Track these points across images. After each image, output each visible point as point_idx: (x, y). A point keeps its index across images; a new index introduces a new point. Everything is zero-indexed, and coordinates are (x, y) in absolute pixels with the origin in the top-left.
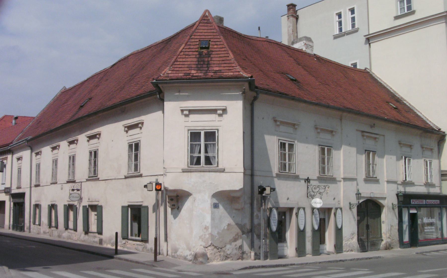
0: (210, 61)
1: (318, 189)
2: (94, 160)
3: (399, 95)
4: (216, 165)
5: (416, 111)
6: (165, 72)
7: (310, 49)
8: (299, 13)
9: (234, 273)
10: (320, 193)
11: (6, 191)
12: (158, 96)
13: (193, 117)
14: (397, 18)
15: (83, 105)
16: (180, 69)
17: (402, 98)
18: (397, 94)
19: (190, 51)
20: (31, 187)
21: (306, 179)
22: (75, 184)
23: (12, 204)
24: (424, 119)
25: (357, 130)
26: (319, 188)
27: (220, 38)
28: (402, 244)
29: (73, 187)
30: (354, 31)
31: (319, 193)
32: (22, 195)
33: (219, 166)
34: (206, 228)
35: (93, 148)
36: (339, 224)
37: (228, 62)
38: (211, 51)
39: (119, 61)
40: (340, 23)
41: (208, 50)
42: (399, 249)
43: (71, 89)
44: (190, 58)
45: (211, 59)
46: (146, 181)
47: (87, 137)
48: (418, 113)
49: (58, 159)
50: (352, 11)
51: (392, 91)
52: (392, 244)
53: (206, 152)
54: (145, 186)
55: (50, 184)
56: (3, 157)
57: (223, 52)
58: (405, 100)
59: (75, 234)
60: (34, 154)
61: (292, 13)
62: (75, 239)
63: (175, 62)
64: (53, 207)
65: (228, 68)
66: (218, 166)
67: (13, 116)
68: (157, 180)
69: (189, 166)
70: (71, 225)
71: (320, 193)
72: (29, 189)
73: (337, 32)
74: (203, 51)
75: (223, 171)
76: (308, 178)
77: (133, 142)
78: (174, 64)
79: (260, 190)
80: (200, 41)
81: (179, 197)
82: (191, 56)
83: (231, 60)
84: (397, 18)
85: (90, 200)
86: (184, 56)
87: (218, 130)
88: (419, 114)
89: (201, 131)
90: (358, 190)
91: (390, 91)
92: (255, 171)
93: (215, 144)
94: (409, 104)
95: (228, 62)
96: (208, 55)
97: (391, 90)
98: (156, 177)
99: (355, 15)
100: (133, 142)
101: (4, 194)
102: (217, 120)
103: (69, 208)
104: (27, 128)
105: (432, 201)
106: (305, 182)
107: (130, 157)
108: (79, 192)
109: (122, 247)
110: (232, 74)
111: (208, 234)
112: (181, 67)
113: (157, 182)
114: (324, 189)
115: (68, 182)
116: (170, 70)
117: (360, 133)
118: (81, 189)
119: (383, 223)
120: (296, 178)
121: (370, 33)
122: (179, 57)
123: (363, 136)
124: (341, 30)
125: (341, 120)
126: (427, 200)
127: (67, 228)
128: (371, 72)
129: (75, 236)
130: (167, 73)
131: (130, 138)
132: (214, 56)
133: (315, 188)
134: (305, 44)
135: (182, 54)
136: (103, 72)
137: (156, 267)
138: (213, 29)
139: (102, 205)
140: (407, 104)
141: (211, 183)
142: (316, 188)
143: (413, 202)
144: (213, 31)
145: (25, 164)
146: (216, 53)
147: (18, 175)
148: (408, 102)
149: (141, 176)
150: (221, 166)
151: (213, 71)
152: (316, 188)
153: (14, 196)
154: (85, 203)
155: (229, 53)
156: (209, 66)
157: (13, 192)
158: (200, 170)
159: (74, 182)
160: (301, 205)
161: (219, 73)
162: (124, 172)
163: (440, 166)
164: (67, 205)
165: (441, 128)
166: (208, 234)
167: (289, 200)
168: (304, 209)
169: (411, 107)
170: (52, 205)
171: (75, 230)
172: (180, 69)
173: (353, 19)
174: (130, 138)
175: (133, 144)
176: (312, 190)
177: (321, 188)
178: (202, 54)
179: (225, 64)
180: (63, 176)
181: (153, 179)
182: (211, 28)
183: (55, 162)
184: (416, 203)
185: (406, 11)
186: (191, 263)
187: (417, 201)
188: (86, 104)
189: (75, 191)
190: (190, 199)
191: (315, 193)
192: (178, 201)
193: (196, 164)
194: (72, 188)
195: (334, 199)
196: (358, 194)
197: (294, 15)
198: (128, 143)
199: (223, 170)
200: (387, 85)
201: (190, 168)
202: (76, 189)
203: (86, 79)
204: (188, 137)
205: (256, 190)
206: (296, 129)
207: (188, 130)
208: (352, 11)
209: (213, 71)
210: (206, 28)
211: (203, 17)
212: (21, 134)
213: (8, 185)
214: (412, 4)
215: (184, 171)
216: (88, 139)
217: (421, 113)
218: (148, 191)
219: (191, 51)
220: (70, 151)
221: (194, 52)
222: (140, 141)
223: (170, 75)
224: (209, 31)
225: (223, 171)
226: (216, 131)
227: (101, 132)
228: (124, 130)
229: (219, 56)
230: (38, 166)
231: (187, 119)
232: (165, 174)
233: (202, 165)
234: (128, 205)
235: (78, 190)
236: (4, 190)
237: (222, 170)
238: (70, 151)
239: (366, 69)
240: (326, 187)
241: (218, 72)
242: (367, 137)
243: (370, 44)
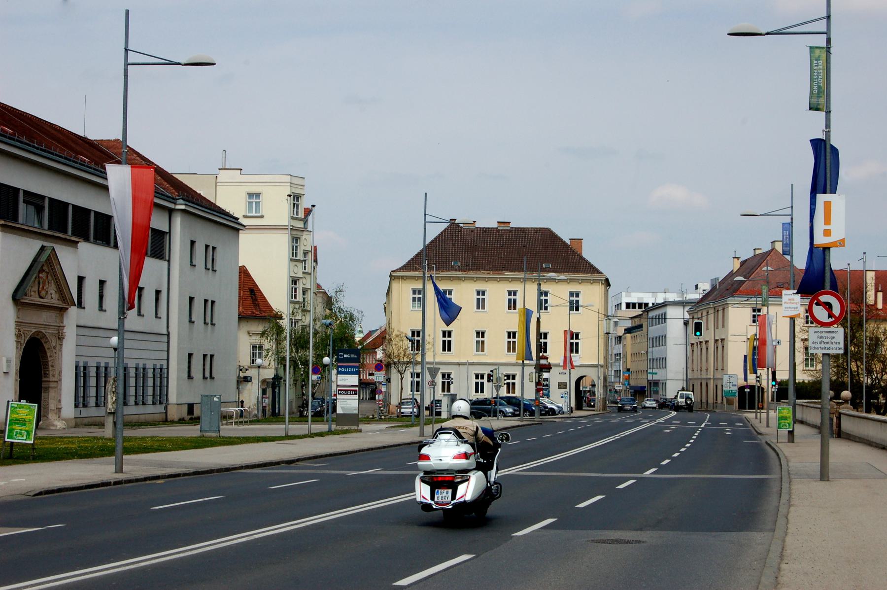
231: (250, 338)
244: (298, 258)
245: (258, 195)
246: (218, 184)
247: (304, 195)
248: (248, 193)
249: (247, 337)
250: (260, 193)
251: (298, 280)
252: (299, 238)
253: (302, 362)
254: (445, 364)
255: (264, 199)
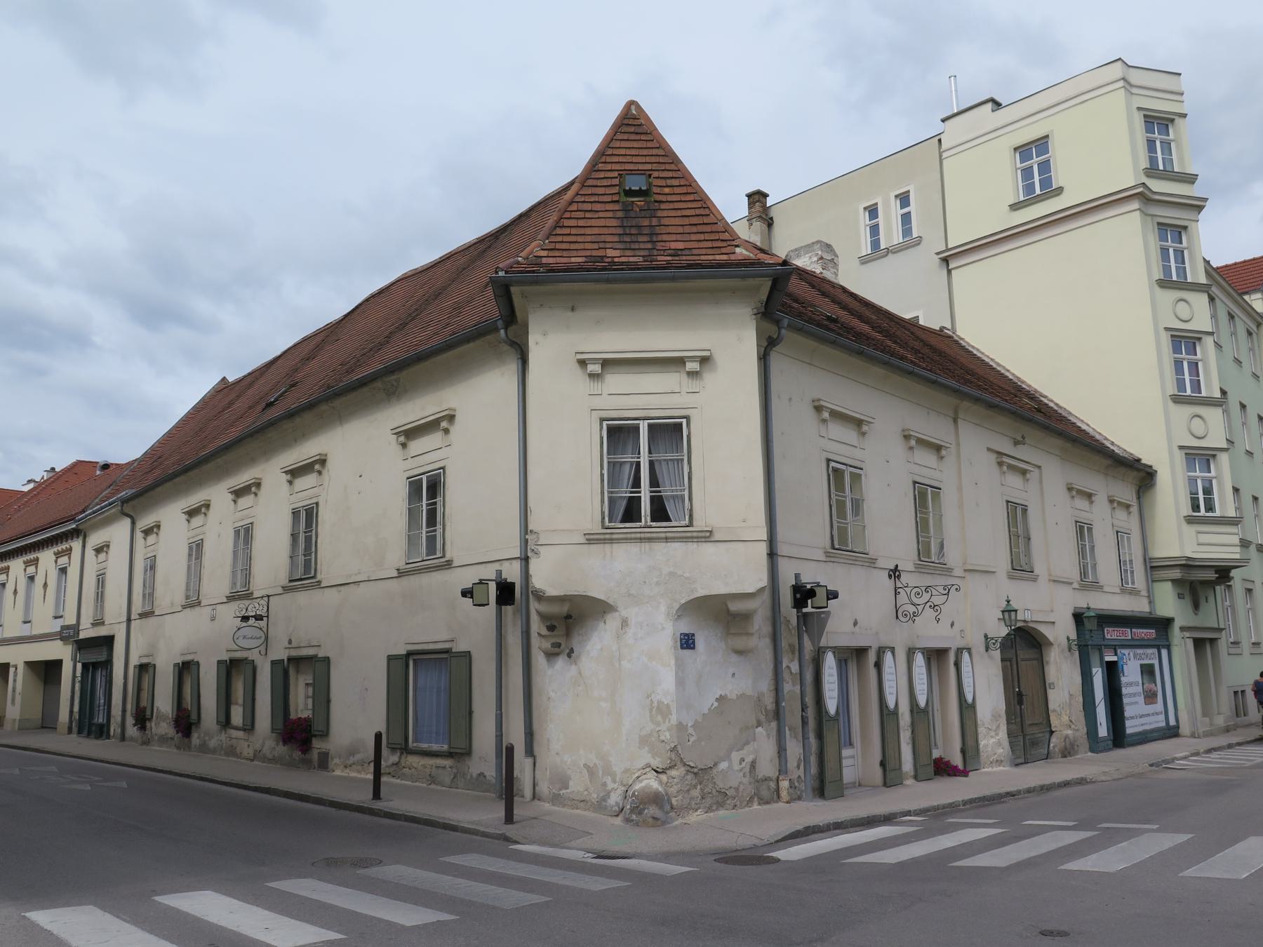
0: (657, 226)
1: (926, 597)
2: (305, 532)
3: (1029, 386)
4: (687, 522)
5: (1073, 420)
6: (531, 254)
7: (832, 270)
8: (774, 213)
9: (784, 854)
10: (933, 607)
11: (64, 635)
12: (502, 332)
13: (617, 382)
14: (1015, 207)
15: (274, 401)
16: (573, 246)
17: (1036, 391)
18: (1023, 382)
19: (597, 200)
20: (129, 620)
21: (891, 570)
22: (250, 601)
23: (79, 666)
24: (1098, 437)
25: (989, 449)
26: (929, 594)
27: (679, 170)
28: (1095, 744)
29: (244, 610)
30: (910, 242)
31: (930, 606)
32: (108, 641)
33: (694, 523)
34: (662, 710)
35: (302, 501)
36: (969, 692)
37: (708, 228)
38: (656, 201)
39: (367, 300)
40: (875, 230)
41: (648, 199)
42: (1089, 754)
43: (239, 381)
44: (598, 218)
45: (659, 221)
46: (468, 578)
47: (286, 472)
48: (1079, 424)
49: (204, 540)
50: (904, 199)
51: (1011, 377)
52: (1076, 743)
53: (654, 482)
54: (466, 593)
55: (180, 609)
56: (60, 549)
57: (690, 205)
58: (1045, 397)
59: (247, 740)
60: (139, 536)
61: (759, 211)
62: (248, 754)
63: (556, 227)
64: (186, 669)
65: (709, 244)
66: (691, 524)
67: (97, 463)
68: (499, 573)
69: (607, 523)
70: (237, 716)
71: (935, 606)
72: (124, 625)
73: (866, 249)
74: (633, 202)
75: (707, 537)
76: (897, 566)
77: (423, 474)
78: (554, 233)
79: (798, 596)
80: (620, 178)
81: (571, 620)
82: (600, 213)
83: (717, 223)
84: (1015, 207)
85: (294, 645)
86: (581, 214)
87: (687, 418)
88: (1084, 427)
89: (641, 422)
90: (1008, 602)
91: (1007, 377)
92: (778, 544)
93: (682, 460)
94: (1056, 404)
95: (708, 228)
96: (649, 211)
97: (1007, 374)
98: (497, 566)
99: (912, 208)
100: (423, 474)
101: (59, 643)
102: (685, 389)
103: (231, 668)
104: (127, 475)
105: (1141, 631)
106: (890, 576)
107: (412, 514)
108: (263, 623)
109: (389, 773)
110: (725, 257)
111: (669, 730)
112: (576, 242)
113: (499, 580)
114: (946, 596)
115: (231, 598)
116: (542, 249)
117: (993, 457)
118: (268, 617)
119: (1050, 688)
120: (872, 563)
121: (949, 247)
122: (567, 215)
123: (1000, 464)
124: (875, 244)
125: (955, 420)
126: (1133, 630)
127: (226, 723)
128: (955, 336)
129: (249, 746)
130: (535, 256)
131: (411, 463)
132: (665, 213)
133: (918, 594)
134: (822, 258)
135: (574, 207)
136: (325, 330)
137: (517, 843)
138: (657, 148)
139: (328, 655)
140: (1051, 405)
141: (671, 574)
142: (921, 593)
143: (1108, 633)
144: (654, 152)
145: (117, 562)
146: (672, 206)
147: (98, 593)
148: (1052, 401)
149: (448, 565)
150: (699, 524)
151: (670, 252)
152: (921, 593)
153: (83, 645)
154: (280, 653)
155: (708, 208)
156: (655, 239)
157: (82, 636)
158: (638, 535)
159: (248, 596)
160: (885, 640)
161: (685, 255)
162: (396, 557)
163: (1198, 540)
164: (226, 661)
165: (1140, 457)
166: (669, 730)
167: (858, 625)
168: (893, 650)
169: (1060, 411)
170: (183, 663)
171: (249, 726)
172: (573, 246)
173: (906, 218)
174: (411, 463)
175: (422, 479)
176: (910, 599)
177: (934, 592)
178: (632, 210)
179: (699, 235)
180: (217, 581)
181: (489, 573)
182: (649, 144)
183: (196, 549)
184: (1113, 637)
185: (1038, 192)
186: (618, 821)
187: (1116, 632)
188: (282, 398)
189: (252, 621)
190: (612, 622)
191: (920, 608)
192: (568, 634)
193: (624, 520)
194: (243, 613)
195: (952, 625)
196: (1010, 611)
197: (764, 216)
198: (408, 478)
199: (708, 534)
200: (998, 364)
201: (609, 531)
202: (254, 614)
203: (279, 353)
204: (602, 438)
205: (786, 597)
206: (864, 434)
207: (602, 420)
208: (904, 199)
209: (670, 252)
210: (635, 145)
211: (625, 118)
212: (109, 490)
213: (70, 619)
214: (1052, 174)
215: (591, 540)
216: (289, 477)
217: (1088, 425)
218: (474, 605)
219: (598, 202)
220: (239, 515)
221: (607, 205)
222: (443, 468)
223: (544, 260)
224: (645, 152)
225: (707, 537)
226: (684, 421)
227: (326, 455)
228: (395, 442)
229: (679, 213)
230: (152, 567)
231: (595, 387)
232: (535, 550)
233: (646, 522)
234: (407, 651)
235: (258, 618)
236: (60, 633)
237: (703, 534)
238: (239, 515)
239: (942, 329)
240: (949, 590)
241: (684, 253)
242: (1010, 467)
243: (949, 272)
244: (1218, 513)
245: (1042, 144)
246: (945, 155)
247: (1184, 116)
248: (1015, 149)
249: (582, 385)
250: (1047, 136)
251: (1199, 339)
252: (1185, 228)
253: (996, 734)
254: (132, 566)
255: (1059, 155)
